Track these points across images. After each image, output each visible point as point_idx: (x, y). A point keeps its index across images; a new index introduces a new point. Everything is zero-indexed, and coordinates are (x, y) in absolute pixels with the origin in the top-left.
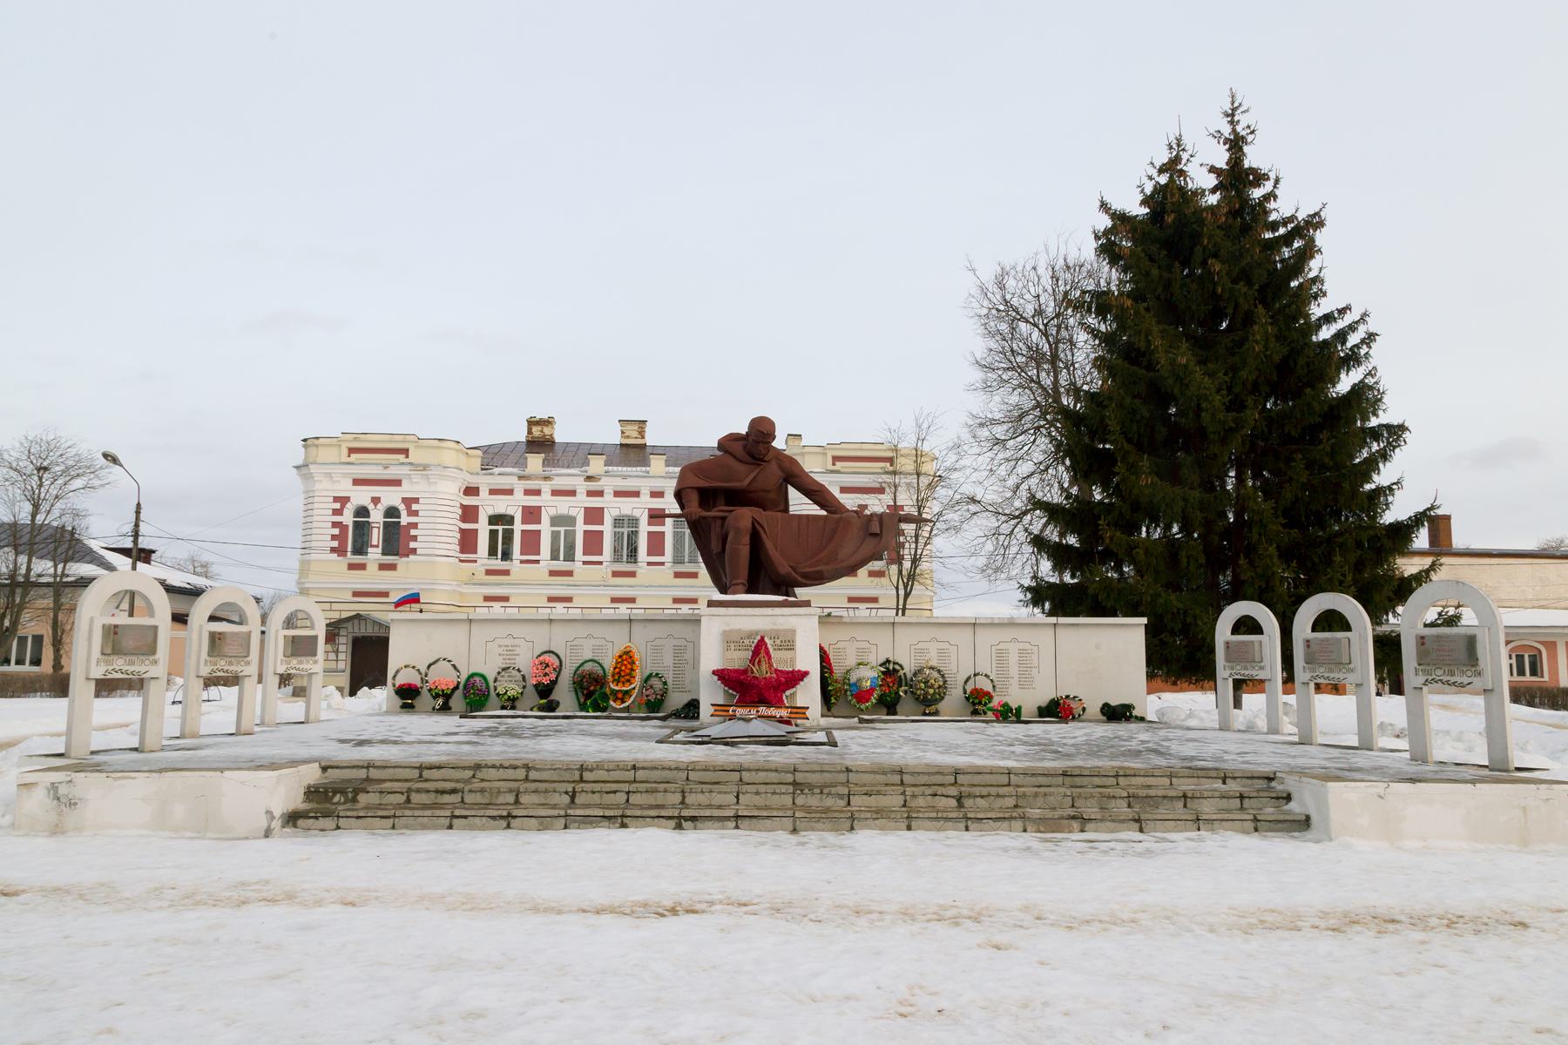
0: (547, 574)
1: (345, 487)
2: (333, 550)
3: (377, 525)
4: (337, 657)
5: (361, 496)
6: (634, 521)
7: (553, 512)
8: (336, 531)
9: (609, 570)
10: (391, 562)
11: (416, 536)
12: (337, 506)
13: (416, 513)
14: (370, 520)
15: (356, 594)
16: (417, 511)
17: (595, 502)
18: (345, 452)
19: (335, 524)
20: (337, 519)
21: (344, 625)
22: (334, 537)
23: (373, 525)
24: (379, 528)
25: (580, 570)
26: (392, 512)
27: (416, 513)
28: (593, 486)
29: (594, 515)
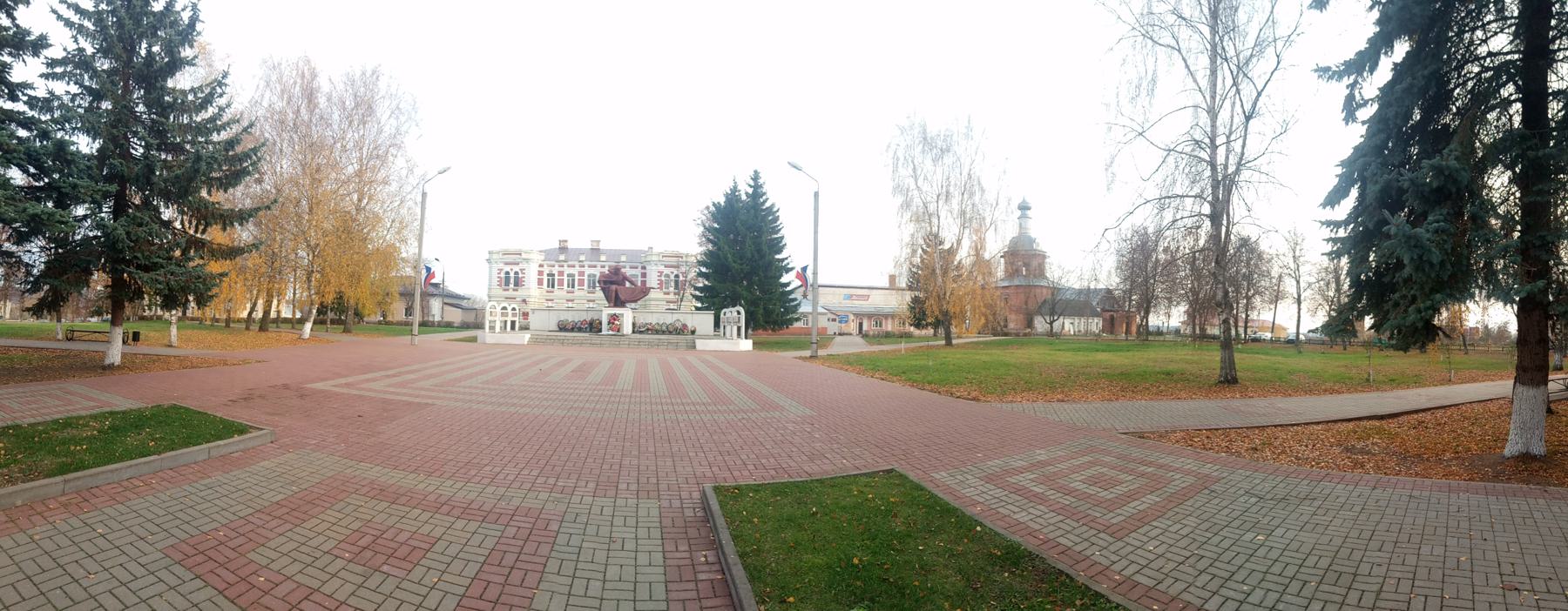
1: (501, 266)
5: (507, 268)
26: (516, 273)
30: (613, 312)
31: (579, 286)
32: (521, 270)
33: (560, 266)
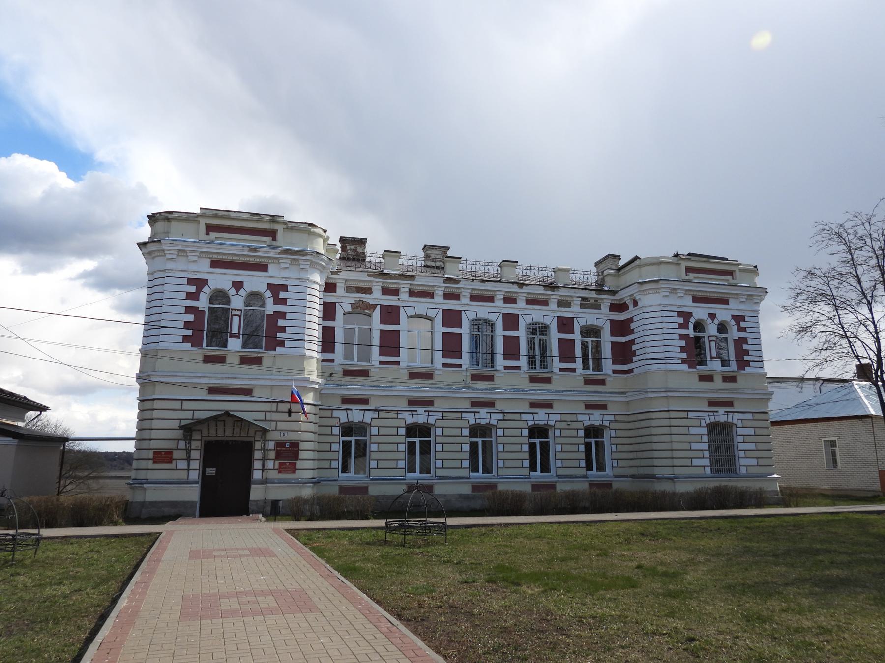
0: (583, 382)
1: (202, 269)
2: (186, 339)
3: (239, 313)
4: (189, 465)
5: (222, 280)
6: (491, 325)
7: (583, 322)
8: (190, 318)
9: (468, 374)
10: (255, 355)
11: (284, 327)
12: (192, 289)
13: (284, 302)
14: (231, 307)
15: (213, 390)
16: (745, 328)
17: (452, 305)
18: (203, 228)
19: (188, 310)
20: (192, 303)
21: (198, 427)
22: (187, 325)
23: (234, 313)
24: (240, 316)
25: (377, 370)
26: (254, 297)
27: (284, 302)
28: (452, 288)
29: (511, 321)
30: (717, 484)
31: (615, 361)
32: (270, 286)
33: (386, 291)
